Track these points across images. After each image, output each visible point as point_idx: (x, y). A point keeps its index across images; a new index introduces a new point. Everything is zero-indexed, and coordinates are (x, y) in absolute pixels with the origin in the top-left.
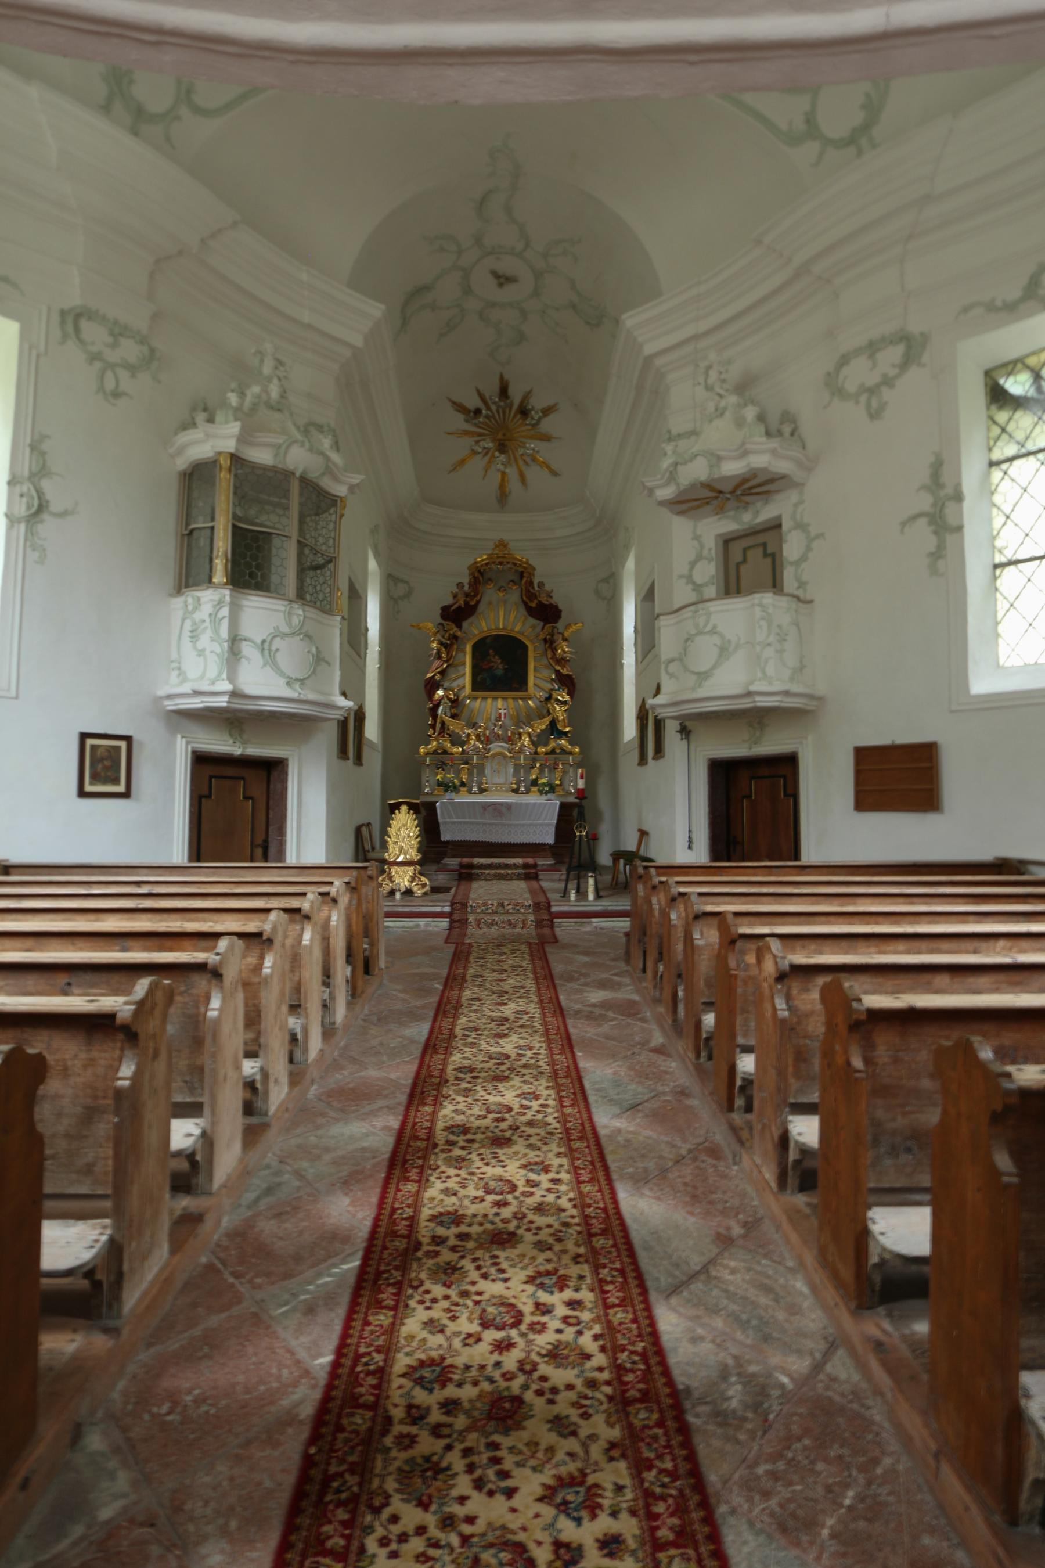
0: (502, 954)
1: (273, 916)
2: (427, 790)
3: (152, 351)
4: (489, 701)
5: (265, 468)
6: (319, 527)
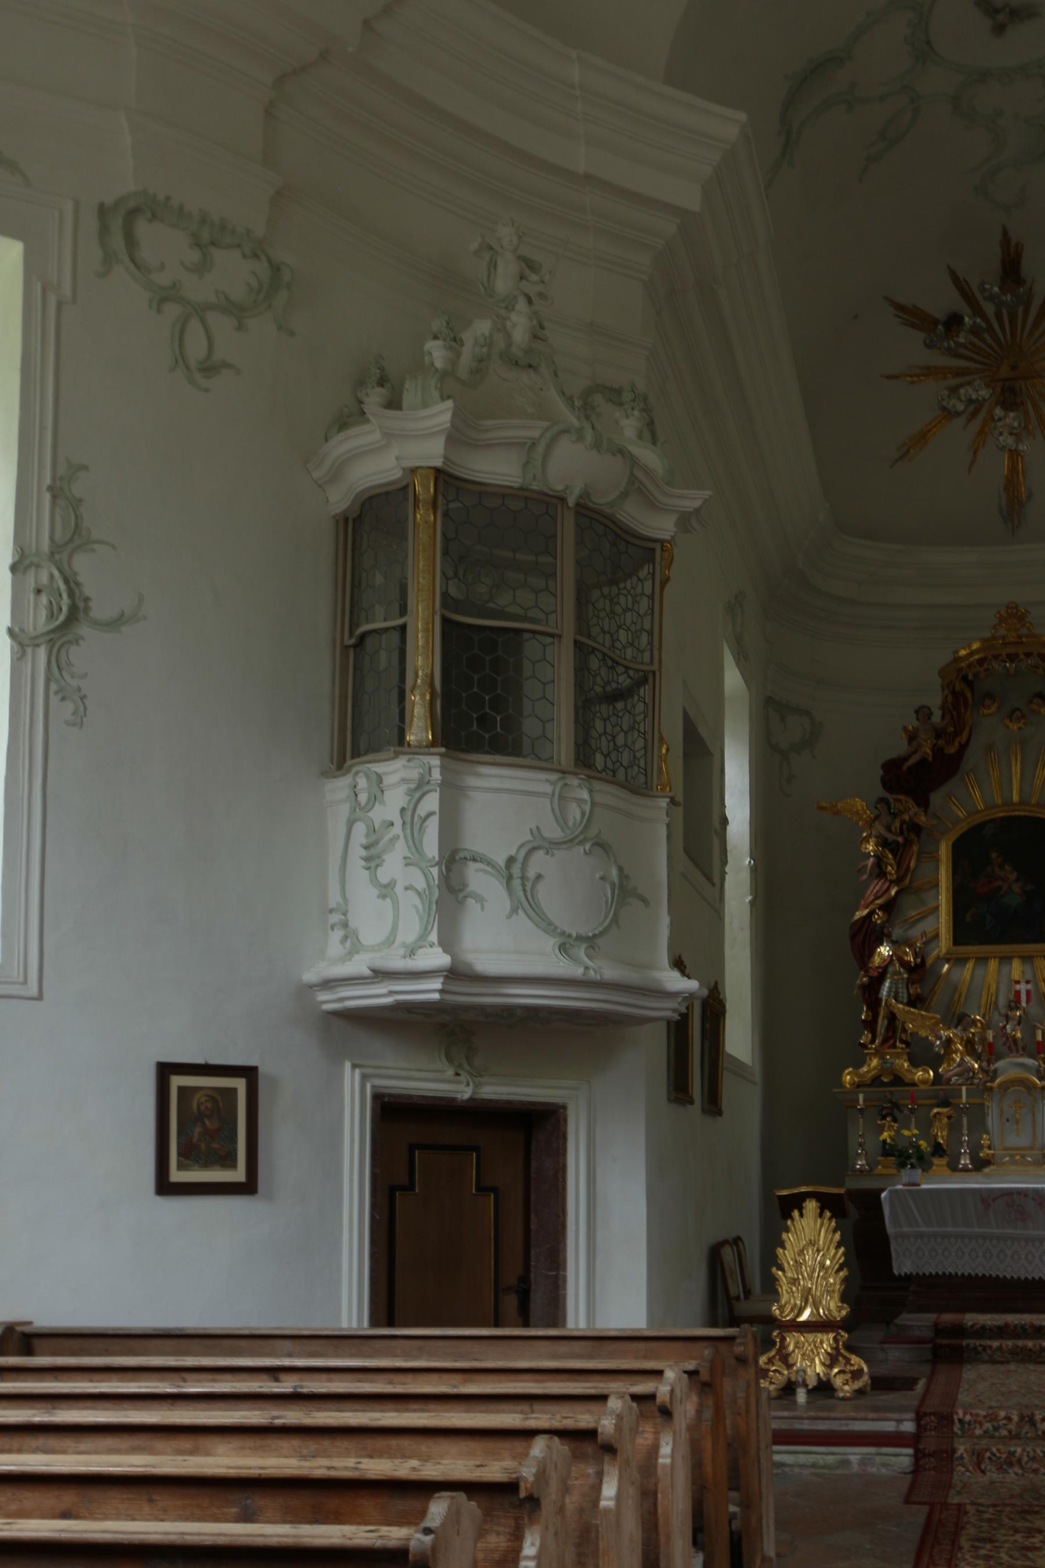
0: (1031, 1532)
1: (538, 1447)
2: (860, 1163)
3: (276, 269)
4: (993, 964)
5: (505, 494)
6: (618, 610)
